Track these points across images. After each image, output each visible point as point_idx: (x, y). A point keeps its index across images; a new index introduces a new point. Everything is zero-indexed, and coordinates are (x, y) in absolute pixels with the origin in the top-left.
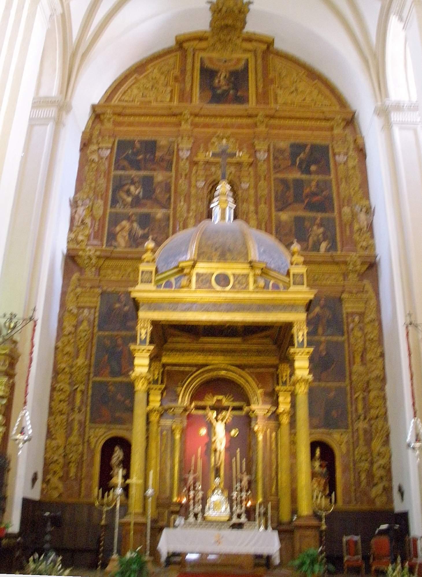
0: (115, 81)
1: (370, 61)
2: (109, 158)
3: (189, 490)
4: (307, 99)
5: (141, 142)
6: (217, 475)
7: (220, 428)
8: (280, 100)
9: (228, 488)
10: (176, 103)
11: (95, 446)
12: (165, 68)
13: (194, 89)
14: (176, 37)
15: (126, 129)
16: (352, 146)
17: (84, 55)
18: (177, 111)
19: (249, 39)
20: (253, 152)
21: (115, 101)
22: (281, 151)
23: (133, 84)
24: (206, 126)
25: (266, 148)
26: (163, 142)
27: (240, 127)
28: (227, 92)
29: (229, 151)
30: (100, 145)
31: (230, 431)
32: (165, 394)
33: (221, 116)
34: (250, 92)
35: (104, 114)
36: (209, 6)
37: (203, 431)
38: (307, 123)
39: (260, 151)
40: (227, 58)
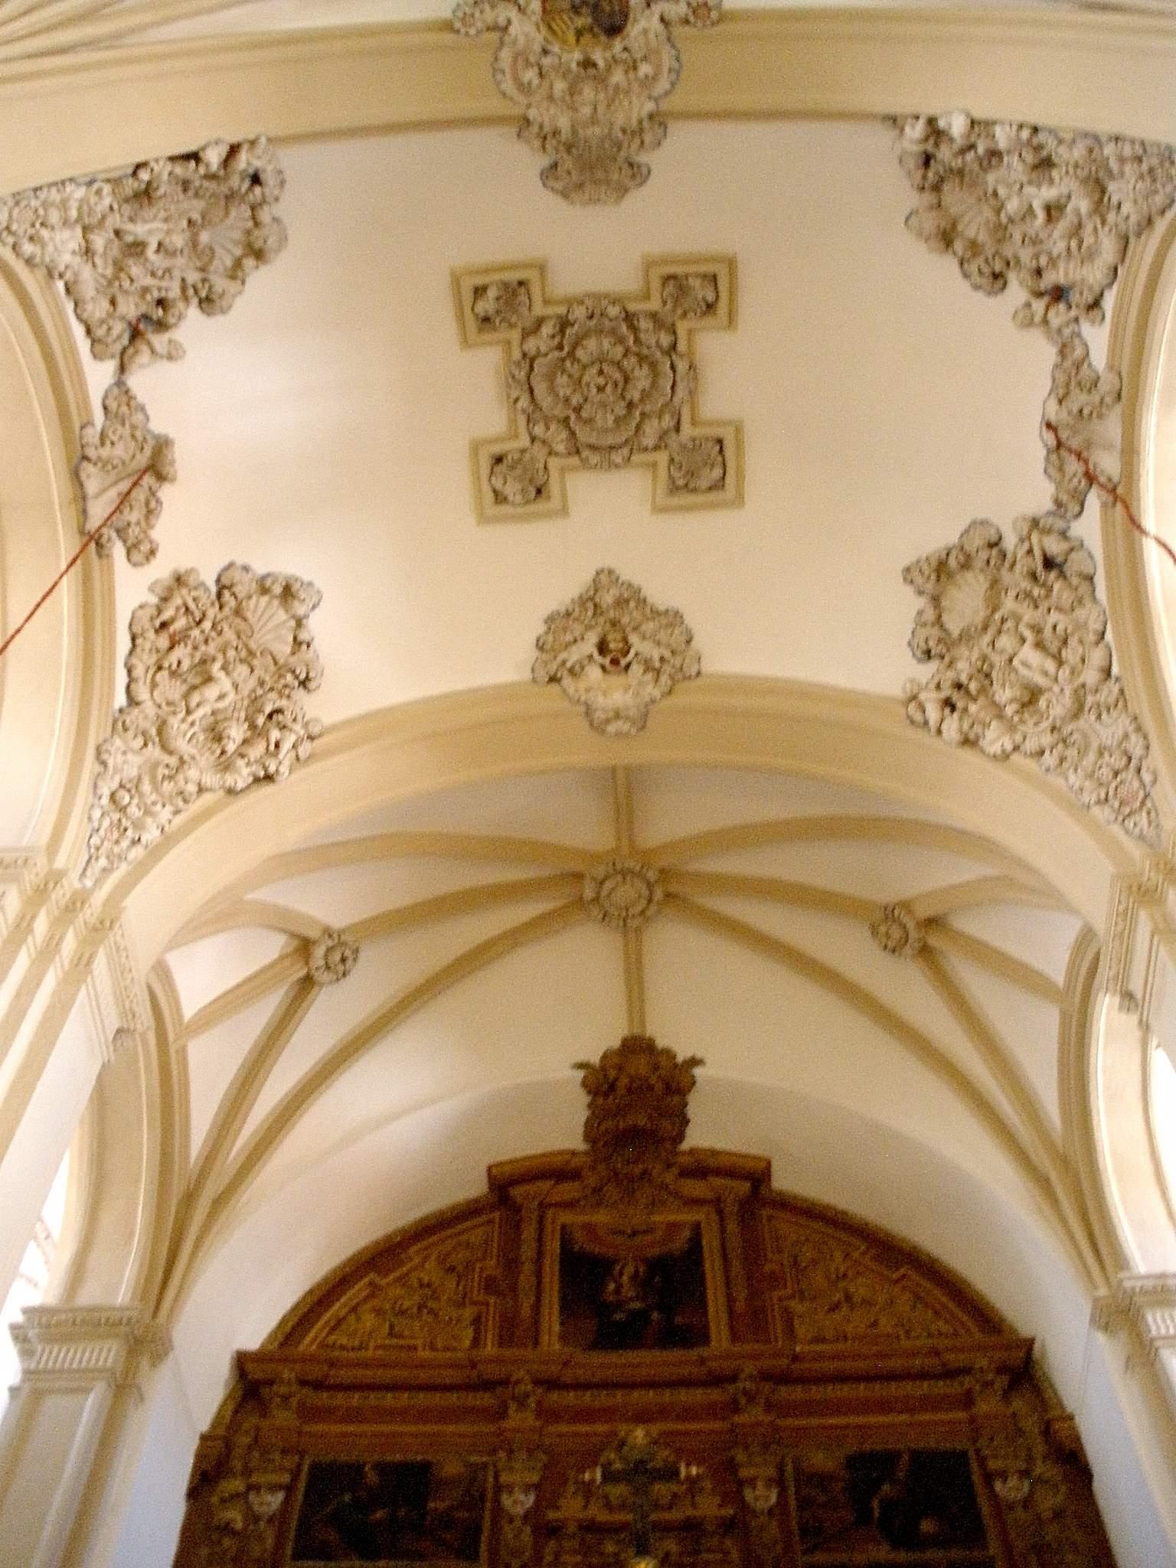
0: (311, 1292)
1: (1054, 1177)
2: (279, 1519)
4: (883, 1321)
5: (382, 1468)
8: (801, 1330)
10: (490, 1349)
12: (459, 1258)
13: (545, 1311)
14: (490, 1169)
15: (337, 1428)
16: (1040, 1449)
17: (220, 1202)
18: (492, 1371)
19: (704, 1167)
20: (729, 1480)
21: (308, 1344)
22: (823, 1480)
23: (366, 1299)
24: (588, 1415)
25: (771, 1472)
26: (451, 1468)
27: (688, 1413)
28: (642, 1316)
29: (658, 1463)
30: (255, 1479)
33: (632, 1386)
34: (711, 1310)
35: (270, 1383)
36: (580, 1074)
38: (893, 1389)
39: (752, 1482)
40: (638, 1224)
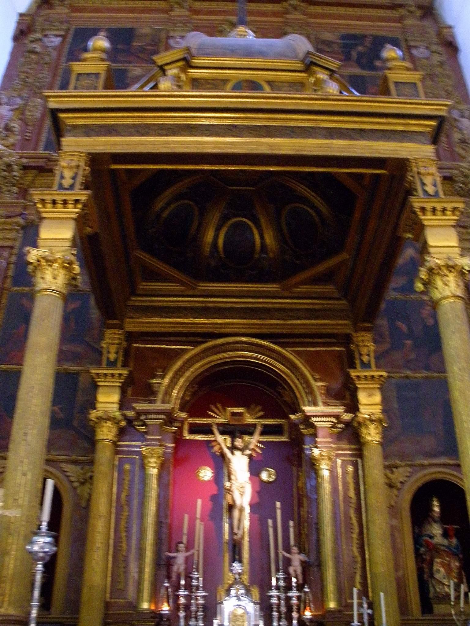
3: (177, 587)
6: (236, 556)
7: (239, 463)
9: (259, 581)
32: (130, 391)
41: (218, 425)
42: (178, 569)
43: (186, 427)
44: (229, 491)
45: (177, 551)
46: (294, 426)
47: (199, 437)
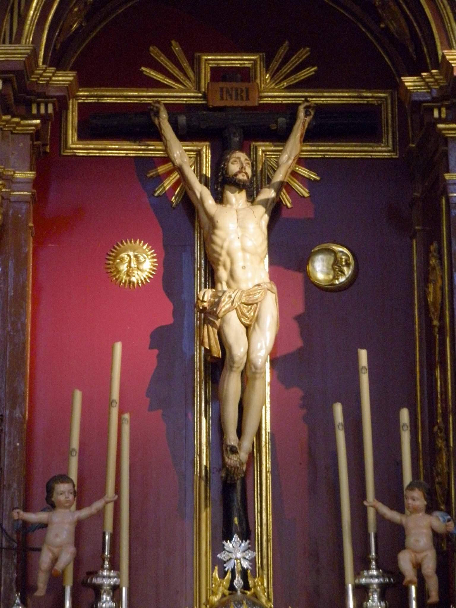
6: (234, 519)
7: (241, 231)
11: (206, 172)
31: (302, 264)
37: (139, 263)
41: (174, 110)
42: (55, 560)
43: (72, 117)
44: (210, 315)
45: (52, 506)
46: (414, 111)
47: (115, 149)
